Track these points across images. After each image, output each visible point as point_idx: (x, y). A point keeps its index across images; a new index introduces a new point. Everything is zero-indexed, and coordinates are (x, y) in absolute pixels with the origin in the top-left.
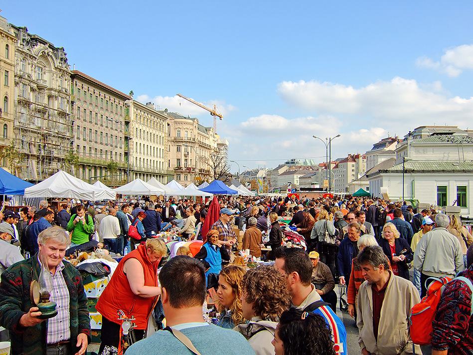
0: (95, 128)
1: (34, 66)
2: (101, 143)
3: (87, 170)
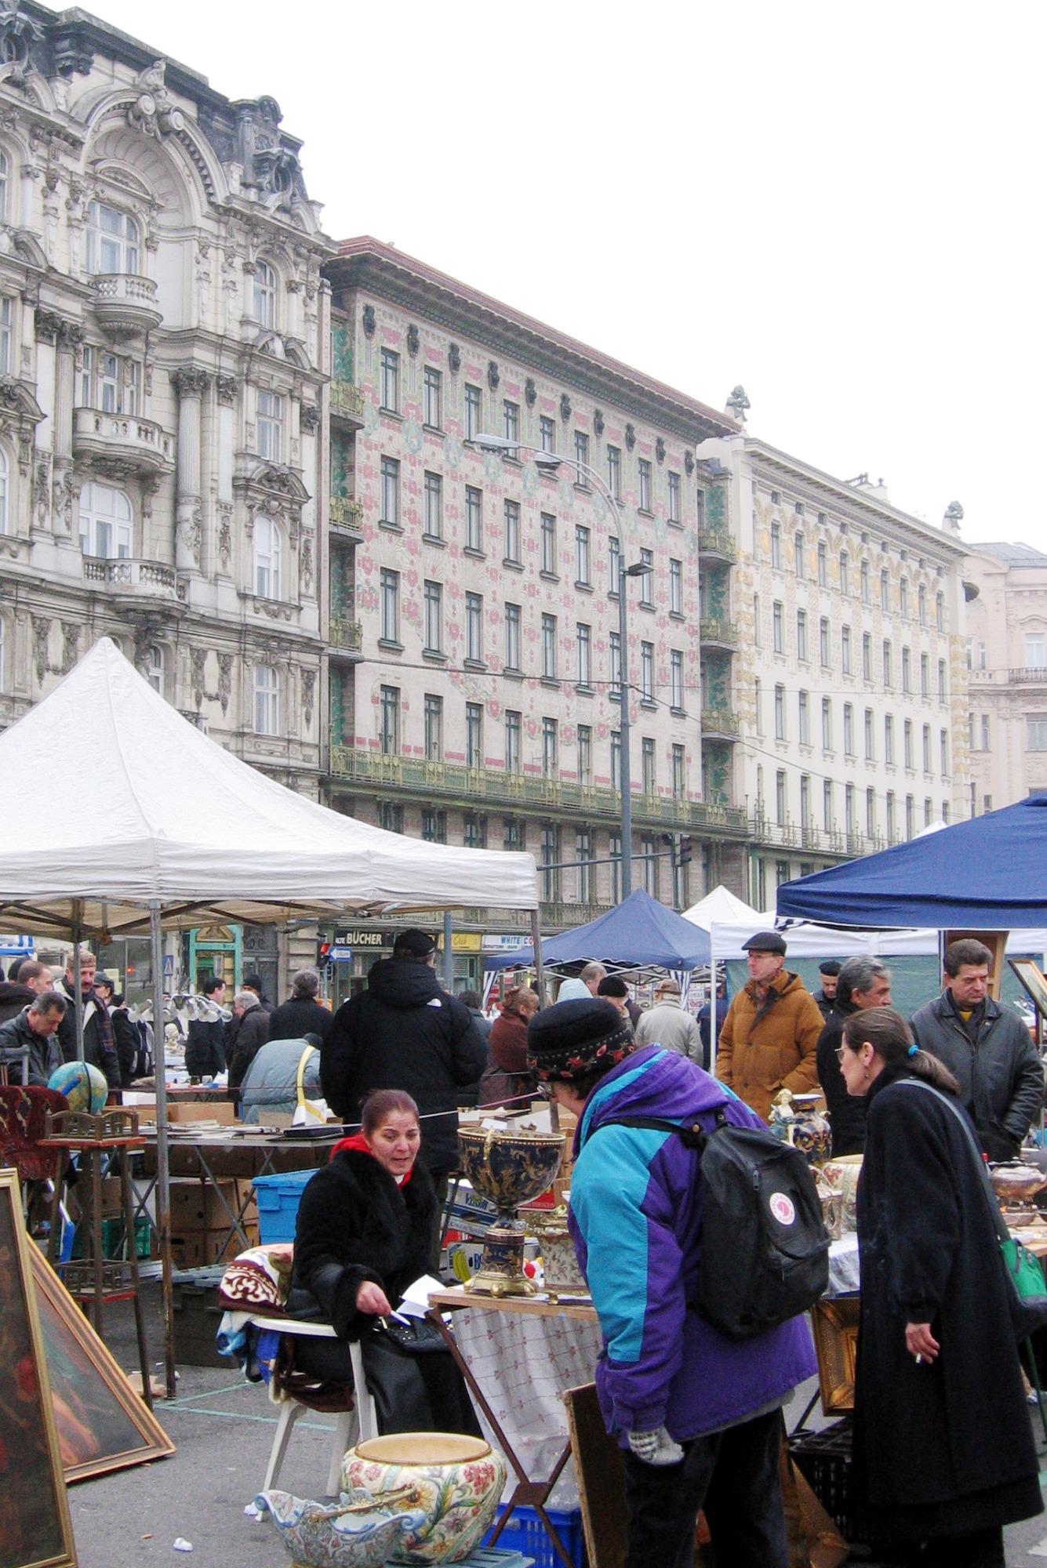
0: (499, 590)
1: (63, 190)
2: (550, 682)
3: (569, 854)
